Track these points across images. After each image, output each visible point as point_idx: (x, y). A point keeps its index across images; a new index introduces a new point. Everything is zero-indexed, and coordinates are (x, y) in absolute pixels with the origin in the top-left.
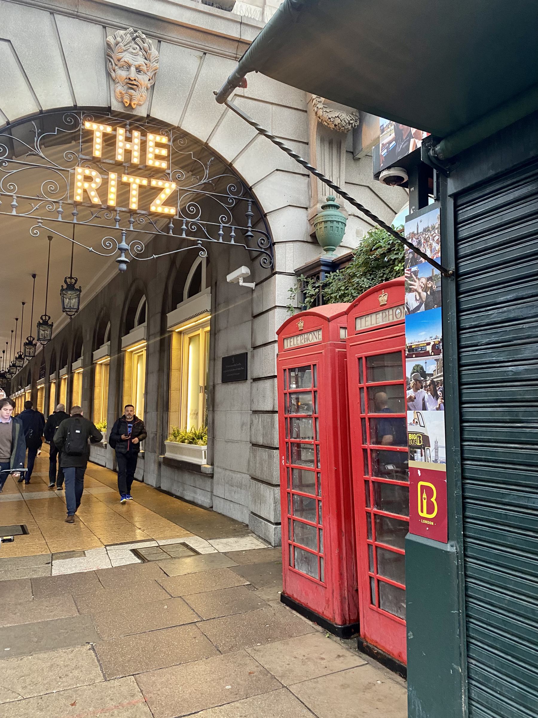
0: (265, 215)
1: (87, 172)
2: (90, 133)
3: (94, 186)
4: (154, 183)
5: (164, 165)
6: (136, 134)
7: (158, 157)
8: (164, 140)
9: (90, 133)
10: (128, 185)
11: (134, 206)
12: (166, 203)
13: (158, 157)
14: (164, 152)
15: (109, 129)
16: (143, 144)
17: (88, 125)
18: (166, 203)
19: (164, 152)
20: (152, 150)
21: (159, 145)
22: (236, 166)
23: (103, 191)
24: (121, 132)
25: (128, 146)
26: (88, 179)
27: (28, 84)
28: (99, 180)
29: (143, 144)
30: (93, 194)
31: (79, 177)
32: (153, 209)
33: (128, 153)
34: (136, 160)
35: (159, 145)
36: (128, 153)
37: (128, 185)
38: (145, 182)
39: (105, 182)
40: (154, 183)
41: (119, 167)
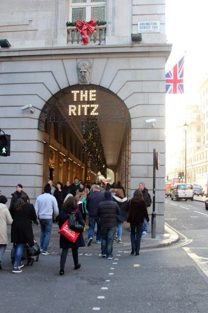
0: (53, 95)
1: (72, 106)
2: (73, 94)
3: (74, 110)
4: (92, 106)
5: (95, 99)
6: (86, 91)
7: (93, 97)
8: (95, 91)
9: (73, 94)
10: (84, 108)
11: (86, 114)
12: (95, 112)
13: (93, 97)
14: (95, 95)
15: (78, 92)
16: (88, 95)
17: (72, 92)
18: (95, 112)
19: (95, 95)
20: (91, 95)
21: (93, 93)
22: (118, 95)
23: (77, 112)
24: (82, 91)
25: (84, 95)
26: (72, 108)
27: (18, 59)
28: (75, 108)
29: (88, 95)
30: (74, 112)
31: (70, 108)
32: (91, 114)
33: (84, 98)
34: (86, 100)
35: (93, 93)
36: (84, 98)
37: (84, 108)
38: (89, 106)
39: (77, 109)
40: (92, 106)
41: (84, 102)
